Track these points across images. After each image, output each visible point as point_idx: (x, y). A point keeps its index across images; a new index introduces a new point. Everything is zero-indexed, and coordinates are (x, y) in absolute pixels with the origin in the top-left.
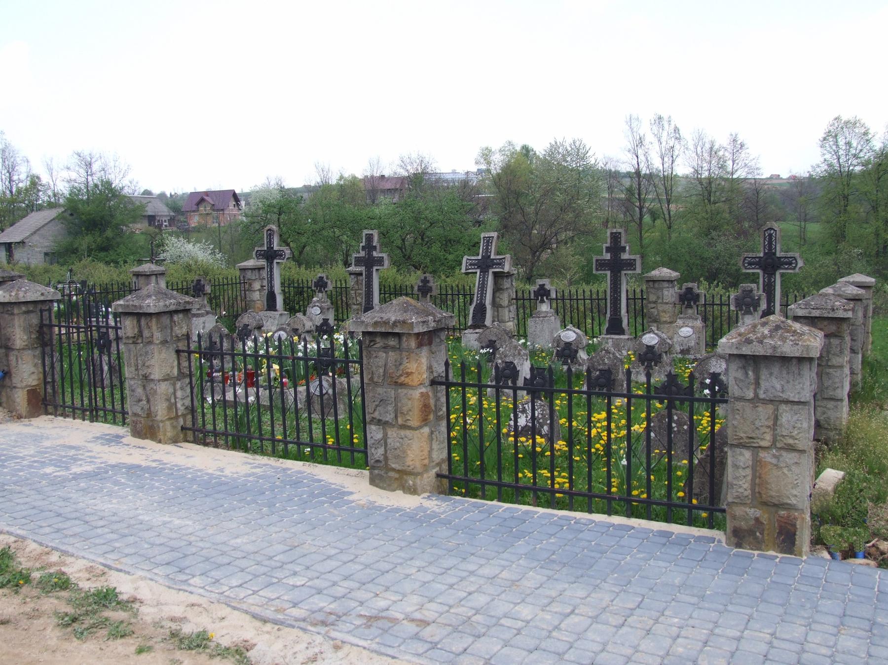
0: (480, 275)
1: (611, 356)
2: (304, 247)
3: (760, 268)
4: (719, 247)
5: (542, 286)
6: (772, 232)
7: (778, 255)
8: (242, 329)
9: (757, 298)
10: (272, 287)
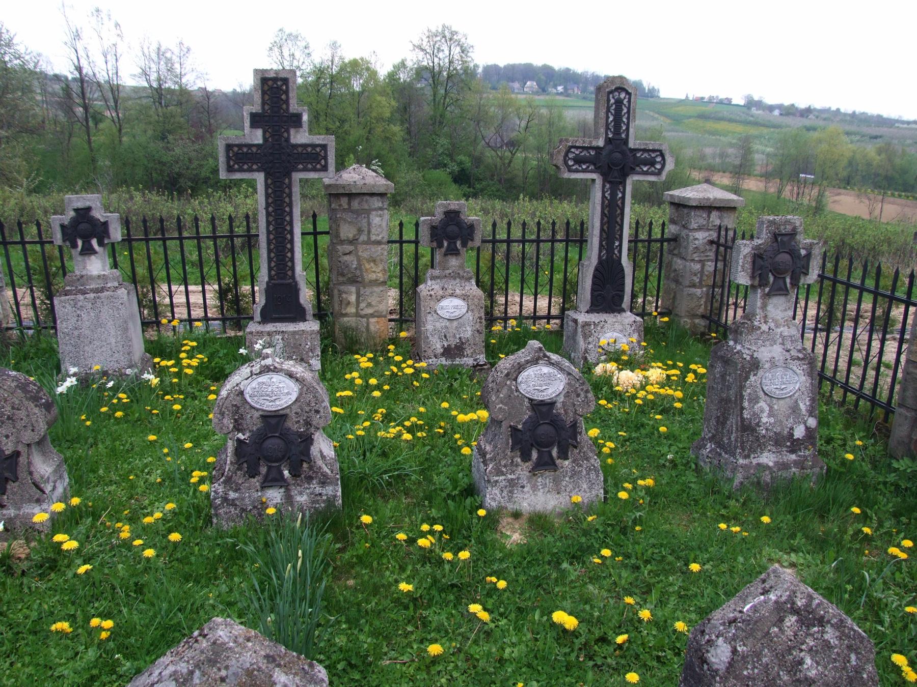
1: (830, 635)
3: (597, 170)
4: (178, 151)
6: (623, 95)
9: (803, 252)
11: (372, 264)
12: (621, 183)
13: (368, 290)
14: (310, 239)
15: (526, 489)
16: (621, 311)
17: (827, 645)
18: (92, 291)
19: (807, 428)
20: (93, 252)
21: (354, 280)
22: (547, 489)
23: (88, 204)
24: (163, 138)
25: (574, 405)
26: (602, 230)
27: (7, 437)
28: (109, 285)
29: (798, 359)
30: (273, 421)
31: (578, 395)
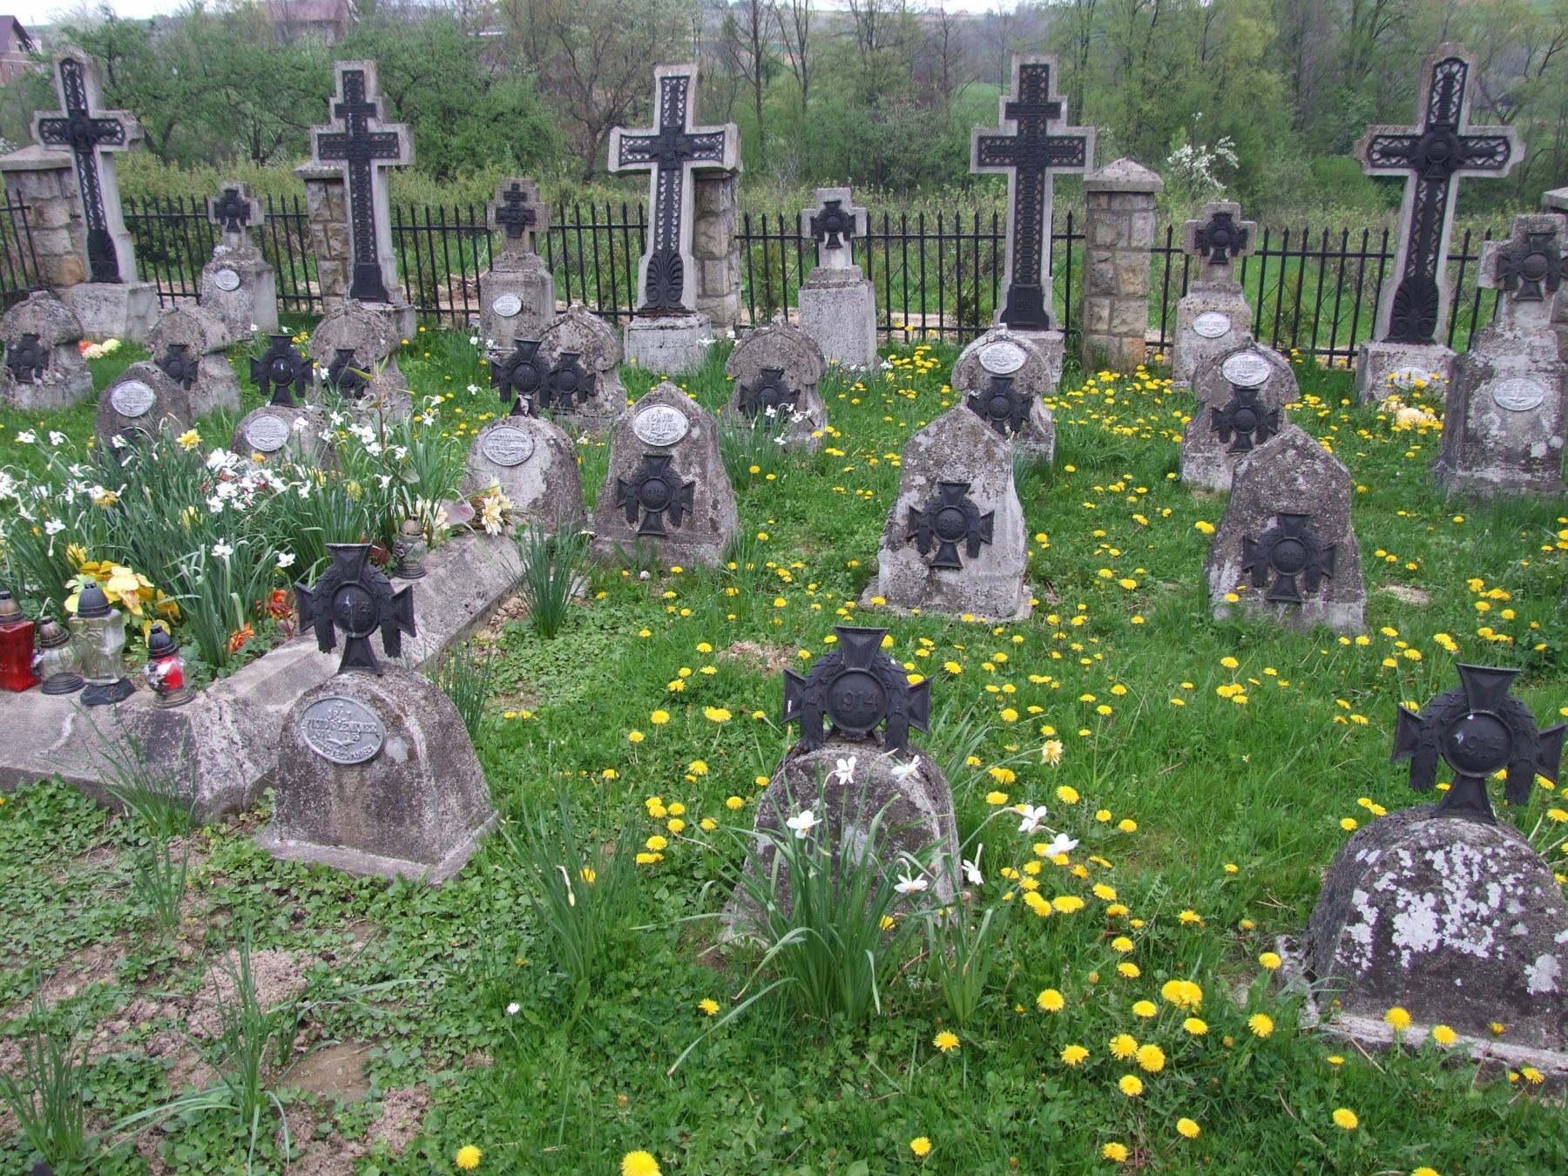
0: (660, 177)
1: (1319, 466)
2: (171, 125)
3: (1412, 164)
5: (833, 207)
6: (1455, 68)
7: (1463, 130)
8: (21, 350)
10: (98, 219)
12: (1442, 181)
13: (1124, 305)
14: (1061, 245)
16: (1430, 342)
17: (1316, 472)
18: (834, 285)
19: (1549, 448)
20: (839, 246)
21: (1107, 293)
23: (838, 197)
24: (871, 100)
26: (1412, 240)
29: (1546, 370)
30: (1002, 383)
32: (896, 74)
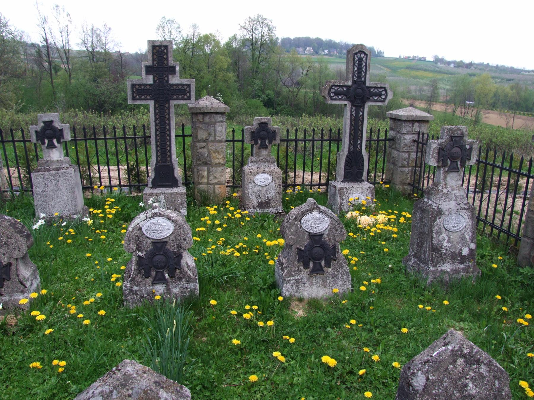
3: (348, 99)
4: (103, 88)
6: (363, 55)
9: (468, 147)
11: (217, 154)
12: (361, 106)
13: (214, 169)
14: (181, 139)
15: (306, 285)
16: (361, 181)
17: (481, 376)
19: (470, 249)
20: (54, 147)
21: (206, 163)
22: (318, 285)
23: (51, 119)
24: (95, 80)
25: (334, 236)
26: (350, 134)
27: (4, 254)
28: (63, 166)
29: (465, 209)
31: (337, 230)
32: (104, 72)
